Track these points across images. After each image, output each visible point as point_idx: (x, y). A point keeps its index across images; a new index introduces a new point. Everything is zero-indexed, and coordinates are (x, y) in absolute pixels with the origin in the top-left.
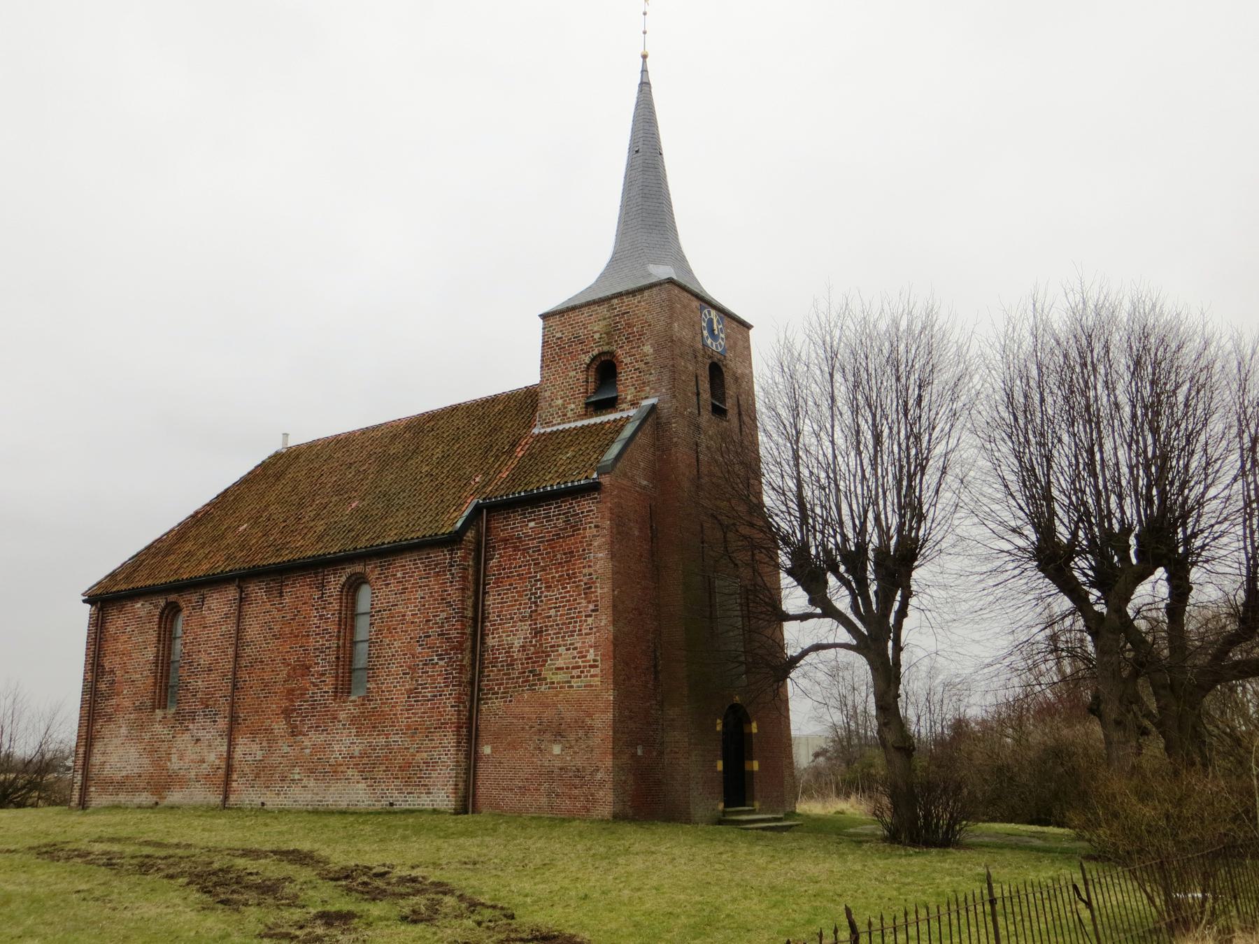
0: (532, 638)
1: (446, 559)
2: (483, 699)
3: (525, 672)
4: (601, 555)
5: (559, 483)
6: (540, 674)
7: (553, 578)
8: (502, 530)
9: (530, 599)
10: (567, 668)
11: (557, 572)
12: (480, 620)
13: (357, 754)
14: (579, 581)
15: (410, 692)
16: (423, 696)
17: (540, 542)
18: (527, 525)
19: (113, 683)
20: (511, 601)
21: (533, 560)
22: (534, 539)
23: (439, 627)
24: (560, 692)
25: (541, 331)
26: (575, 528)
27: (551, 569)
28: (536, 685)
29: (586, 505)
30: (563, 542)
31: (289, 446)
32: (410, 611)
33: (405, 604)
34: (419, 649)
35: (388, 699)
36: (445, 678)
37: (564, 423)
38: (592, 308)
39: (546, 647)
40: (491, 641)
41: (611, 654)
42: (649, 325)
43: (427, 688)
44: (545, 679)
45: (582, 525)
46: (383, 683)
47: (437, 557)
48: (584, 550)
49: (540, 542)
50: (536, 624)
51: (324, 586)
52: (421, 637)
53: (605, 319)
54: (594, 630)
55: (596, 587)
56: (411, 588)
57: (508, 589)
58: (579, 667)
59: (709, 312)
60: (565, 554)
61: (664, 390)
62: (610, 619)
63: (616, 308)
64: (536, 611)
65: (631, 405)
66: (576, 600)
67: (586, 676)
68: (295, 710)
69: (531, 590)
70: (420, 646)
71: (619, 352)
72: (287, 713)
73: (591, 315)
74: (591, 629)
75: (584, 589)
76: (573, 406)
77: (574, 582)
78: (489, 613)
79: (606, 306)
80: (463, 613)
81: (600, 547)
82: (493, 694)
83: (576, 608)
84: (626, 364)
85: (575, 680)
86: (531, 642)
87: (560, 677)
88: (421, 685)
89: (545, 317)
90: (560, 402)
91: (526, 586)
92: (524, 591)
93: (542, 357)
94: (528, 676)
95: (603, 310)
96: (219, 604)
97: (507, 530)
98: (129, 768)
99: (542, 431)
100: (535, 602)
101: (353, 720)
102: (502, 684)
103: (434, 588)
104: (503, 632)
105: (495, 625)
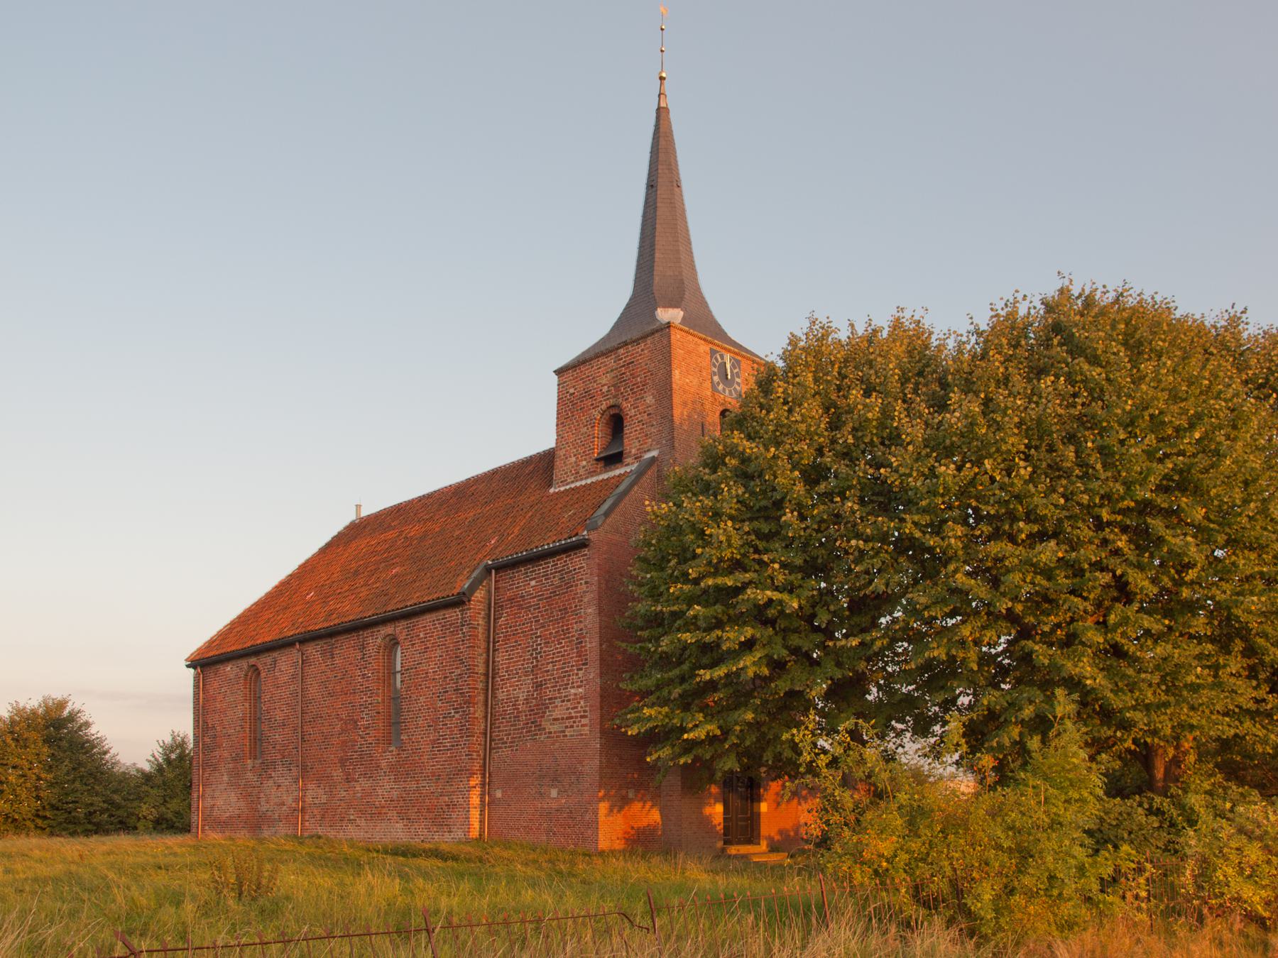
0: (534, 691)
1: (458, 619)
2: (494, 748)
3: (528, 723)
4: (590, 610)
5: (554, 542)
6: (540, 725)
7: (551, 634)
8: (508, 590)
9: (532, 655)
10: (563, 719)
11: (554, 629)
12: (490, 675)
13: (395, 798)
14: (572, 636)
15: (434, 742)
16: (444, 746)
17: (540, 600)
18: (529, 584)
19: (215, 737)
20: (516, 657)
21: (534, 618)
22: (535, 597)
23: (454, 683)
24: (556, 741)
25: (557, 387)
26: (569, 585)
27: (549, 626)
28: (537, 734)
29: (578, 562)
30: (559, 599)
31: (362, 516)
32: (432, 669)
33: (428, 662)
34: (440, 704)
35: (417, 749)
36: (460, 730)
37: (577, 481)
38: (601, 360)
39: (545, 700)
40: (501, 695)
41: (598, 704)
42: (652, 375)
43: (446, 739)
44: (544, 729)
45: (574, 582)
46: (413, 735)
47: (451, 617)
48: (576, 606)
49: (540, 600)
50: (537, 678)
51: (364, 648)
52: (440, 693)
53: (612, 371)
54: (584, 682)
55: (586, 642)
56: (432, 647)
57: (513, 646)
58: (572, 718)
59: (722, 357)
60: (560, 610)
61: (664, 442)
62: (598, 671)
63: (622, 359)
64: (537, 666)
65: (636, 458)
66: (569, 654)
67: (578, 726)
68: (348, 759)
69: (533, 646)
70: (441, 700)
71: (624, 404)
72: (343, 762)
73: (600, 368)
74: (582, 682)
75: (576, 644)
76: (584, 463)
77: (568, 638)
78: (499, 669)
79: (613, 357)
80: (474, 669)
81: (589, 602)
82: (503, 743)
83: (569, 663)
84: (631, 417)
85: (569, 729)
86: (533, 695)
87: (556, 727)
88: (442, 736)
89: (559, 372)
90: (574, 459)
91: (529, 643)
92: (527, 647)
93: (558, 414)
94: (531, 727)
95: (610, 361)
96: (286, 663)
97: (513, 589)
98: (231, 809)
99: (557, 490)
100: (536, 658)
101: (392, 768)
102: (510, 734)
103: (449, 647)
104: (510, 687)
105: (503, 680)
